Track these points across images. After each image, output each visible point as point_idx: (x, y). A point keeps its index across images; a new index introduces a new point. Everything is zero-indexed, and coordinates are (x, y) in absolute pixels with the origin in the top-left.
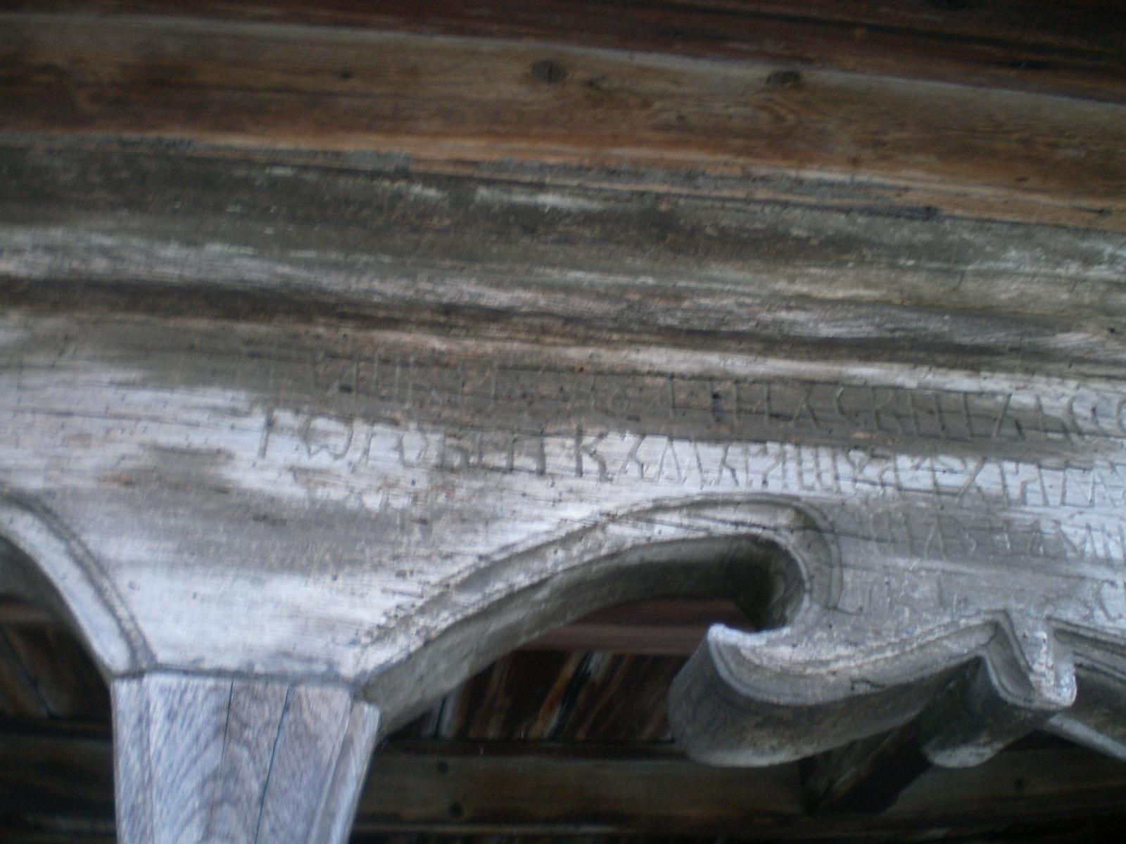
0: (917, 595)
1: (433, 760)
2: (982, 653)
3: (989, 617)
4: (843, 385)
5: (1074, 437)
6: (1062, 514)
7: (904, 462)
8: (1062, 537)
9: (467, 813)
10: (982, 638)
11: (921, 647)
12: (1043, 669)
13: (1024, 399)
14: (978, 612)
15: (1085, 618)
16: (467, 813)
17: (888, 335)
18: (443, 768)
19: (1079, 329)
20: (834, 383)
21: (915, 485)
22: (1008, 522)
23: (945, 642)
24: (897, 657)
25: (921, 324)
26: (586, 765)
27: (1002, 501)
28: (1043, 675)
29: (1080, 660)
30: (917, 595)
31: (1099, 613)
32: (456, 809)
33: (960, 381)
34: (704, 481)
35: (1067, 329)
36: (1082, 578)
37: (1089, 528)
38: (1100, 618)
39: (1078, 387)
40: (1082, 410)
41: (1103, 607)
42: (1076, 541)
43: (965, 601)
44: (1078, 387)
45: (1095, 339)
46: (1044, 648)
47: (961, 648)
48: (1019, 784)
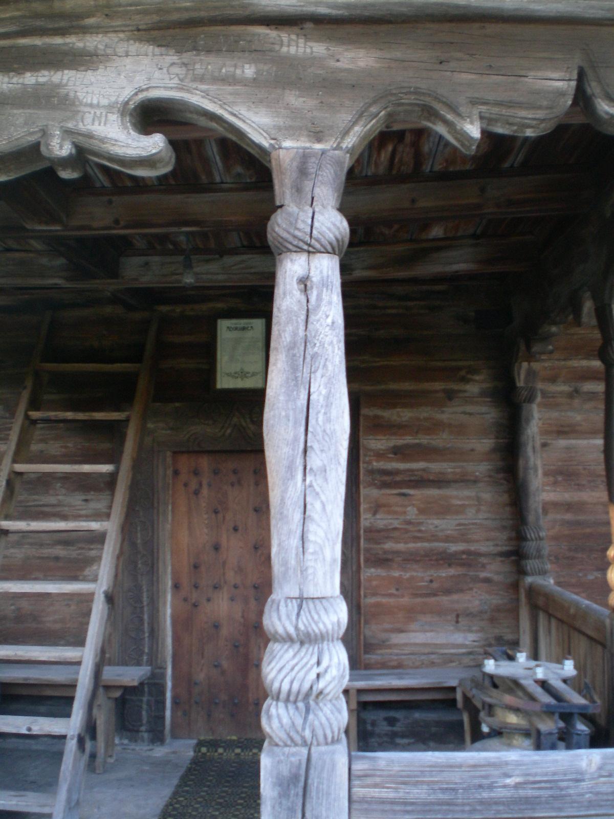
0: (17, 122)
1: (106, 198)
2: (40, 140)
3: (41, 128)
4: (15, 47)
5: (95, 58)
6: (78, 89)
7: (28, 74)
8: (76, 97)
9: (122, 223)
10: (40, 135)
11: (16, 139)
12: (55, 144)
13: (80, 45)
14: (37, 126)
15: (75, 126)
16: (122, 223)
17: (23, 28)
18: (110, 202)
19: (93, 16)
20: (11, 47)
21: (29, 83)
22: (58, 93)
23: (26, 137)
24: (7, 143)
25: (33, 23)
26: (179, 197)
27: (59, 86)
28: (54, 146)
29: (74, 140)
30: (17, 122)
31: (81, 124)
32: (117, 222)
33: (58, 40)
34: (147, 55)
35: (88, 17)
36: (79, 111)
37: (87, 92)
38: (81, 126)
39: (102, 37)
40: (101, 47)
41: (83, 122)
42: (81, 98)
43: (34, 123)
44: (102, 37)
45: (99, 20)
46: (57, 137)
47: (32, 139)
48: (413, 201)
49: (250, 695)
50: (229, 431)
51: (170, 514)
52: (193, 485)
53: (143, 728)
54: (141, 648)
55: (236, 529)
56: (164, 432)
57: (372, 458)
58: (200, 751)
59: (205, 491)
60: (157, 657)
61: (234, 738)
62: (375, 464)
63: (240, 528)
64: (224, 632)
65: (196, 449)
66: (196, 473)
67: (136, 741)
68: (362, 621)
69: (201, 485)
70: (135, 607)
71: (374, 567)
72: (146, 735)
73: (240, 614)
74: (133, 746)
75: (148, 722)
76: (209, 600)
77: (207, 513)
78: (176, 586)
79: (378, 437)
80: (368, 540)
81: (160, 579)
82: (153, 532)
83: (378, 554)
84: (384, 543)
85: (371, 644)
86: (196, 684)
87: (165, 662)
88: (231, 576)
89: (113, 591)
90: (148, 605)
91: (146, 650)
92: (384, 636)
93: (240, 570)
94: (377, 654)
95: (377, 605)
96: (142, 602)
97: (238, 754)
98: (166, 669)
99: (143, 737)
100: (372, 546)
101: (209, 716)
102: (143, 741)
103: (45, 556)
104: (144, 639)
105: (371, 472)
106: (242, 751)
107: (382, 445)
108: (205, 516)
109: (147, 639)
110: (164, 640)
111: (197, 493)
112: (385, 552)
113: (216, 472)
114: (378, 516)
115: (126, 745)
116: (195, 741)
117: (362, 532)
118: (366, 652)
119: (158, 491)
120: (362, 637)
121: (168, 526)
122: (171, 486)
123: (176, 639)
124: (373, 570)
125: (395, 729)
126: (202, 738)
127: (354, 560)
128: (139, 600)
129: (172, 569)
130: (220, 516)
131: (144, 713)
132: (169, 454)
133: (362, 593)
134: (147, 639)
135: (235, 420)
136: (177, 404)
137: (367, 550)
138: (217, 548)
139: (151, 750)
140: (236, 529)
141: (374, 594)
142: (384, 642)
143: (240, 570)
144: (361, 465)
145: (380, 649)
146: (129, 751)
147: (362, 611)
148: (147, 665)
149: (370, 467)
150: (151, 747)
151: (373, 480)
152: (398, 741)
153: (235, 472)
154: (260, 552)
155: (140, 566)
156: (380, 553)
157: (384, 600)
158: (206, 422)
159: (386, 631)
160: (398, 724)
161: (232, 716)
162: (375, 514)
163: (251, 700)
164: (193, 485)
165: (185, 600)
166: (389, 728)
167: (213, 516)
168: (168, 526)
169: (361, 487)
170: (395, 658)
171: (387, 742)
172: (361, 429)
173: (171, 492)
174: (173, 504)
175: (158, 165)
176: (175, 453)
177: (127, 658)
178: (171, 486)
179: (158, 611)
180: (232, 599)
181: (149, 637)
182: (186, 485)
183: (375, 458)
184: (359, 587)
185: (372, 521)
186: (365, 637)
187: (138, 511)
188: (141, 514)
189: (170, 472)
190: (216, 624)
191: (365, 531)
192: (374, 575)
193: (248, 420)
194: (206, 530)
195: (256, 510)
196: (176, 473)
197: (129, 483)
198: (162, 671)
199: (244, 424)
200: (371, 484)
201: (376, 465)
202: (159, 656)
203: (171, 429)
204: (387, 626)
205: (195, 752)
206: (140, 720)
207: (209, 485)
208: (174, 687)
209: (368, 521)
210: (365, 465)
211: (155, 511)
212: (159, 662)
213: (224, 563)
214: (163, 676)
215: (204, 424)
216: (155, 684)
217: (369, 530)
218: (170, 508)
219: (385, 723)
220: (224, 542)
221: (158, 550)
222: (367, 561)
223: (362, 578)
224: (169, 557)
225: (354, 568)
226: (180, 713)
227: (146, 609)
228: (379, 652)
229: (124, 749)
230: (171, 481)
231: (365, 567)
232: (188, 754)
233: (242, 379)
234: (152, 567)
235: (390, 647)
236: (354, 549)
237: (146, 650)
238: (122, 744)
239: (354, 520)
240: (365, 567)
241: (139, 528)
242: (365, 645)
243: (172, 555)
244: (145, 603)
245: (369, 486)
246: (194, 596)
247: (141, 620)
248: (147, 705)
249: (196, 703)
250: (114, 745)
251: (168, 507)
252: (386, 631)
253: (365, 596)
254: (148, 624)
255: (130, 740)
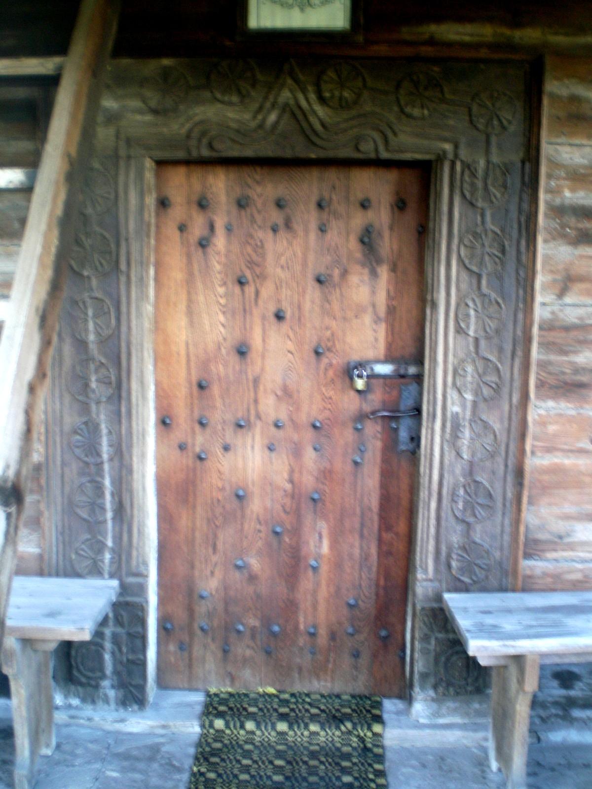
49: (301, 619)
50: (273, 117)
51: (152, 283)
52: (198, 229)
53: (106, 683)
54: (100, 538)
55: (279, 317)
56: (139, 117)
57: (562, 182)
58: (211, 725)
59: (220, 241)
60: (129, 555)
61: (271, 690)
62: (567, 194)
63: (288, 315)
64: (255, 506)
65: (206, 153)
66: (202, 204)
67: (93, 702)
68: (525, 500)
69: (212, 227)
70: (87, 464)
71: (554, 398)
72: (112, 693)
73: (286, 476)
74: (88, 711)
75: (116, 672)
76: (226, 448)
77: (224, 284)
78: (164, 423)
79: (577, 141)
80: (546, 345)
81: (134, 412)
82: (118, 319)
83: (563, 373)
84: (576, 352)
85: (536, 541)
86: (202, 597)
87: (146, 564)
88: (269, 406)
89: (18, 474)
90: (111, 460)
91: (110, 543)
92: (560, 526)
93: (287, 394)
94: (547, 560)
95: (555, 470)
96: (99, 455)
97: (282, 734)
98: (147, 576)
99: (106, 695)
100: (553, 357)
101: (225, 652)
102: (106, 701)
103: (531, 139)
104: (105, 521)
105: (559, 211)
106: (291, 727)
107: (583, 158)
108: (221, 290)
109: (110, 524)
110: (142, 509)
111: (203, 244)
112: (577, 370)
113: (242, 204)
114: (568, 300)
115: (77, 708)
116: (198, 698)
117: (535, 330)
118: (528, 556)
119: (127, 240)
120: (522, 529)
121: (149, 309)
122: (153, 229)
123: (166, 518)
124: (551, 404)
125: (572, 693)
126: (213, 690)
127: (517, 384)
128: (93, 449)
129: (157, 392)
130: (250, 290)
131: (107, 657)
132: (149, 164)
133: (528, 448)
134: (110, 524)
135: (286, 95)
136: (166, 62)
137: (542, 365)
138: (242, 352)
139: (122, 721)
140: (279, 317)
141: (549, 450)
142: (561, 537)
143: (287, 394)
144: (542, 196)
145: (555, 550)
146: (82, 721)
147: (526, 482)
148: (112, 576)
149: (558, 201)
150: (122, 713)
151: (563, 226)
152: (577, 713)
153: (279, 204)
154: (325, 361)
155: (94, 385)
156: (568, 371)
157: (567, 461)
158: (226, 98)
159: (567, 517)
160: (579, 685)
161: (268, 653)
162: (561, 294)
163: (302, 627)
164: (198, 229)
165: (182, 447)
166: (563, 692)
167: (237, 289)
168: (149, 309)
169: (540, 239)
170: (580, 566)
171: (557, 716)
172: (545, 121)
173: (153, 242)
174: (158, 265)
175: (104, 693)
176: (161, 163)
177: (73, 557)
178: (153, 229)
179: (130, 471)
180: (271, 449)
181: (113, 519)
182: (182, 228)
183: (567, 183)
184: (523, 436)
185: (556, 308)
186: (527, 527)
187: (89, 277)
188: (94, 282)
189: (151, 200)
190: (241, 493)
191: (541, 328)
192: (552, 413)
193: (312, 96)
194: (222, 318)
195: (319, 281)
196: (163, 203)
197: (59, 211)
198: (139, 580)
199: (304, 103)
200: (559, 235)
201: (570, 196)
202: (134, 553)
203: (155, 112)
204: (569, 509)
205: (203, 726)
206: (102, 669)
207: (229, 229)
208: (162, 601)
209: (549, 309)
210: (549, 197)
211: (123, 279)
212: (134, 563)
213: (256, 381)
214: (142, 589)
215: (222, 102)
216: (127, 604)
217: (548, 327)
218: (152, 272)
219: (555, 683)
220: (256, 340)
221: (129, 355)
222: (540, 385)
223: (530, 419)
224: (150, 367)
225: (516, 399)
226: (172, 647)
227: (106, 467)
228: (550, 555)
229: (72, 717)
230: (153, 221)
231: (538, 397)
232: (191, 730)
233: (302, 10)
234: (119, 386)
235: (571, 547)
236: (517, 362)
237: (110, 543)
238: (70, 706)
239: (521, 306)
240: (538, 397)
241: (90, 312)
242: (526, 545)
243: (155, 365)
244: (105, 456)
245: (554, 239)
246: (200, 440)
247: (99, 489)
248: (113, 643)
249: (202, 629)
250: (52, 707)
251: (147, 272)
252: (567, 517)
253: (533, 453)
254: (113, 495)
255: (84, 700)
